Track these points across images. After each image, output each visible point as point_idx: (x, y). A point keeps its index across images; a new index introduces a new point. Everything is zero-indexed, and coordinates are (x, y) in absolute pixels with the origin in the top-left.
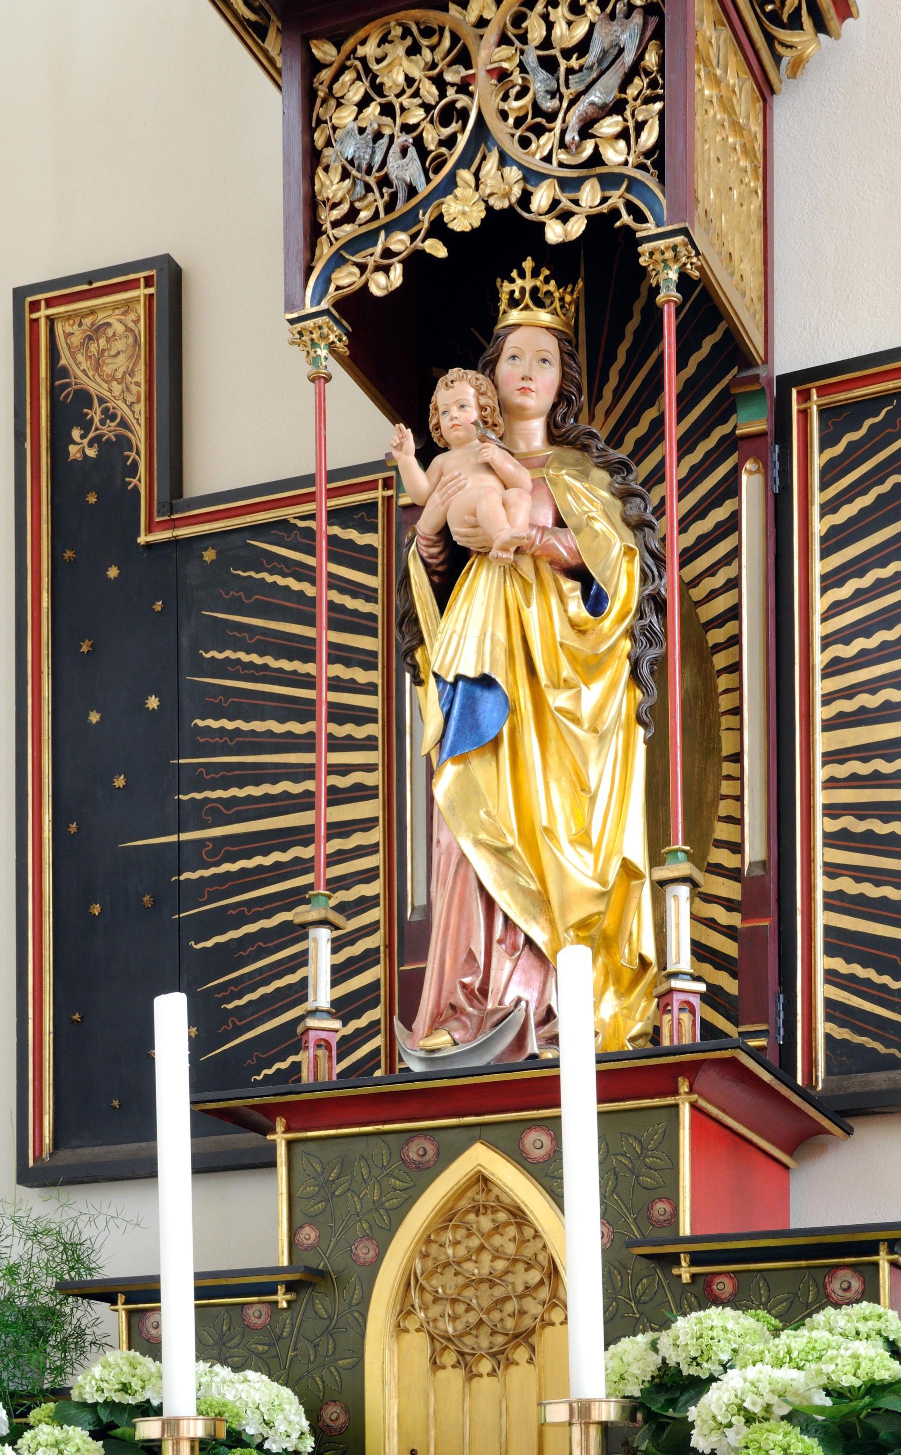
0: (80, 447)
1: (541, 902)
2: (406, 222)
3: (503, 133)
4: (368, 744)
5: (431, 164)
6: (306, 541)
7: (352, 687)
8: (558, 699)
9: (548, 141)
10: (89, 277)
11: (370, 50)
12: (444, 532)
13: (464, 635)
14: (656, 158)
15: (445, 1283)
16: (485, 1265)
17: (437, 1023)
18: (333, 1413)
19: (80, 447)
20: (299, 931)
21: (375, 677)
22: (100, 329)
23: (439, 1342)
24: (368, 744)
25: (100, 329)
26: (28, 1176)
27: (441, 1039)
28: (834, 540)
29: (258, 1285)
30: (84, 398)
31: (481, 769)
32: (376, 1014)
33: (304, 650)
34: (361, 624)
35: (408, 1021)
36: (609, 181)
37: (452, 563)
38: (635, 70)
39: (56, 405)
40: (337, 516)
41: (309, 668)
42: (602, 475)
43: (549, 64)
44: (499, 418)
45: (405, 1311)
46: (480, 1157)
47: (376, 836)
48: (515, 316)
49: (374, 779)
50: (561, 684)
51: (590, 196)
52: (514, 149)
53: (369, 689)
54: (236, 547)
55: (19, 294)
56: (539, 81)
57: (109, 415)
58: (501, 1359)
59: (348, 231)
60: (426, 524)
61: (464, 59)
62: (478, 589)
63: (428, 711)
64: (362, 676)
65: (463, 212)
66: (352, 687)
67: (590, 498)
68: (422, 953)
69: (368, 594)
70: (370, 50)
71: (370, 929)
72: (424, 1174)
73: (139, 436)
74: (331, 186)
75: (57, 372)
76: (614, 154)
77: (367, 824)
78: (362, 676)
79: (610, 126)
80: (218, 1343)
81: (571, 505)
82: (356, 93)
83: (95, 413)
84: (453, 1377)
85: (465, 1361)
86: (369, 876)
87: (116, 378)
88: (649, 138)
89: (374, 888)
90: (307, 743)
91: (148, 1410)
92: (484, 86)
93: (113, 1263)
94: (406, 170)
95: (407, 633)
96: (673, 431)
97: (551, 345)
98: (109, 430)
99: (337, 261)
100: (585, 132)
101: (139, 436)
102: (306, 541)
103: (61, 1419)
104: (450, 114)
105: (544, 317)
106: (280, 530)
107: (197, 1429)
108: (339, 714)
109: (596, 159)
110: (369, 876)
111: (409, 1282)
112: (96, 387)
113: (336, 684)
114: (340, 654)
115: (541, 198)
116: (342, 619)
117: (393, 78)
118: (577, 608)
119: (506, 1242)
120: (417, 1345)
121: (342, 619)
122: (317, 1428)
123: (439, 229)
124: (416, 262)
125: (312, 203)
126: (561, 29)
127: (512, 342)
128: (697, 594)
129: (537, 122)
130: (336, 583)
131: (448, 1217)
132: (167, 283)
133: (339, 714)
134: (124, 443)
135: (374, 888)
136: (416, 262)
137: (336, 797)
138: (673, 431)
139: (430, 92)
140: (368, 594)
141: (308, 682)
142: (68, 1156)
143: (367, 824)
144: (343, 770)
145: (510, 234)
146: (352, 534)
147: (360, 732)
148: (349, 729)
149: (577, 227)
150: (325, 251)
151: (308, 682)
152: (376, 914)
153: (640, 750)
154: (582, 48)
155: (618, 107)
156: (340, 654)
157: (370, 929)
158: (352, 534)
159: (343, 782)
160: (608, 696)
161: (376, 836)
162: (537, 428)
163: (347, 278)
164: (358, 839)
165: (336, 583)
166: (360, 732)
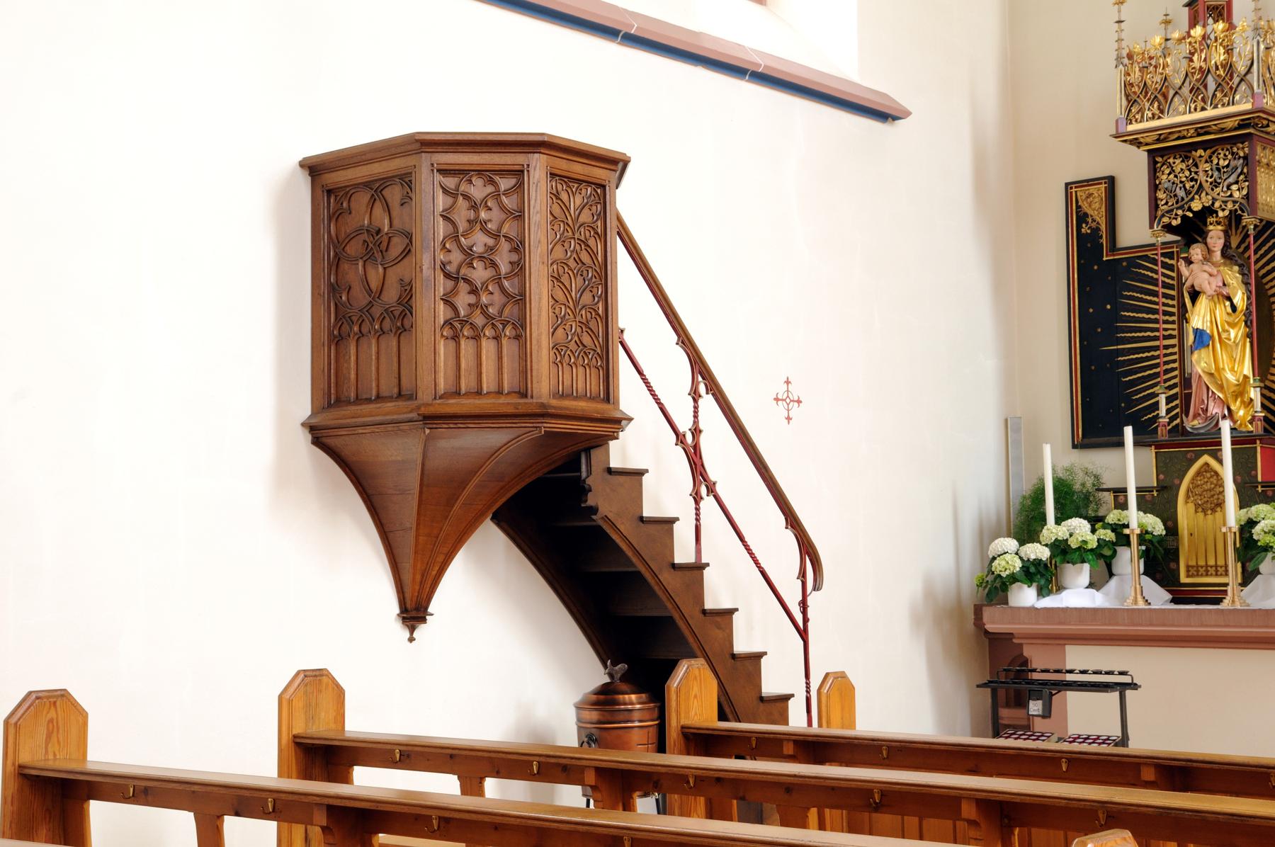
0: (1085, 229)
1: (1221, 388)
2: (1181, 208)
3: (1206, 185)
4: (1173, 322)
5: (1188, 193)
6: (1155, 262)
7: (1168, 305)
8: (1224, 336)
9: (1218, 190)
10: (1087, 181)
11: (1171, 160)
12: (1193, 286)
13: (1200, 317)
14: (1247, 197)
15: (1198, 491)
16: (1208, 486)
17: (1195, 417)
18: (1170, 523)
19: (1085, 229)
20: (1155, 395)
21: (1175, 303)
22: (1090, 195)
23: (1197, 506)
24: (1173, 322)
25: (1090, 195)
26: (1074, 446)
27: (1195, 422)
28: (1257, 261)
29: (1150, 490)
30: (1086, 215)
31: (1204, 352)
32: (1178, 410)
33: (1155, 294)
34: (1171, 287)
35: (1187, 415)
36: (1235, 202)
37: (1195, 295)
38: (1241, 173)
39: (1077, 217)
40: (1163, 255)
41: (1155, 299)
42: (1236, 268)
43: (1218, 170)
44: (1207, 258)
45: (1188, 497)
46: (1206, 458)
47: (1176, 349)
48: (1211, 227)
49: (1175, 333)
50: (1224, 331)
51: (1230, 206)
52: (1209, 191)
53: (1173, 306)
54: (1132, 262)
55: (1067, 184)
56: (1216, 174)
57: (1094, 220)
58: (1213, 510)
59: (1165, 207)
60: (1188, 284)
61: (1196, 165)
62: (1203, 302)
63: (1190, 338)
64: (1171, 302)
65: (1197, 206)
66: (1168, 305)
67: (1233, 276)
68: (1190, 387)
69: (1172, 278)
70: (1171, 160)
71: (1175, 377)
72: (1191, 462)
73: (1103, 227)
74: (1161, 195)
75: (1078, 207)
76: (1236, 195)
77: (1174, 346)
78: (1171, 302)
79: (1234, 187)
80: (1143, 506)
81: (1229, 281)
82: (1167, 171)
83: (1090, 220)
84: (1201, 515)
85: (1204, 511)
86: (1174, 361)
87: (1097, 211)
88: (1245, 192)
89: (1176, 357)
90: (1156, 321)
91: (1127, 526)
92: (1201, 174)
93: (1109, 481)
94: (1181, 193)
95: (1183, 316)
96: (1253, 248)
97: (1222, 234)
98: (1094, 225)
99: (1163, 216)
100: (1228, 187)
101: (1103, 227)
102: (1155, 262)
103: (1104, 528)
104: (1192, 180)
105: (1220, 227)
106: (1146, 258)
107: (1138, 531)
108: (1165, 313)
109: (1231, 196)
110: (1174, 361)
111: (1188, 490)
112: (1090, 212)
113: (1164, 305)
114: (1166, 296)
115: (1217, 204)
116: (1165, 285)
117: (1177, 170)
118: (1229, 310)
119: (1214, 480)
120: (1191, 506)
121: (1165, 285)
122: (1166, 528)
123: (1190, 209)
124: (1184, 217)
125: (1156, 199)
126: (1221, 162)
127: (1210, 234)
128: (1265, 281)
129: (1215, 184)
130: (1164, 275)
131: (1198, 473)
132: (1111, 182)
133: (1165, 313)
134: (1098, 229)
135: (1176, 357)
136: (1184, 217)
137: (1166, 337)
138: (1253, 248)
139: (1187, 173)
140: (1172, 278)
141: (1157, 304)
142: (1086, 441)
143: (1174, 346)
144: (1166, 330)
145: (1208, 211)
146: (1167, 260)
147: (1171, 319)
148: (1167, 318)
149: (1227, 213)
150: (1159, 213)
151: (1157, 304)
152: (1176, 373)
153: (1248, 345)
154: (1227, 166)
155: (1237, 182)
156: (1166, 296)
157: (1175, 377)
158: (1167, 260)
159: (1166, 333)
160: (1236, 333)
161: (1176, 349)
162: (1219, 253)
163: (1166, 220)
164: (1170, 350)
165: (1164, 275)
166: (1171, 319)
